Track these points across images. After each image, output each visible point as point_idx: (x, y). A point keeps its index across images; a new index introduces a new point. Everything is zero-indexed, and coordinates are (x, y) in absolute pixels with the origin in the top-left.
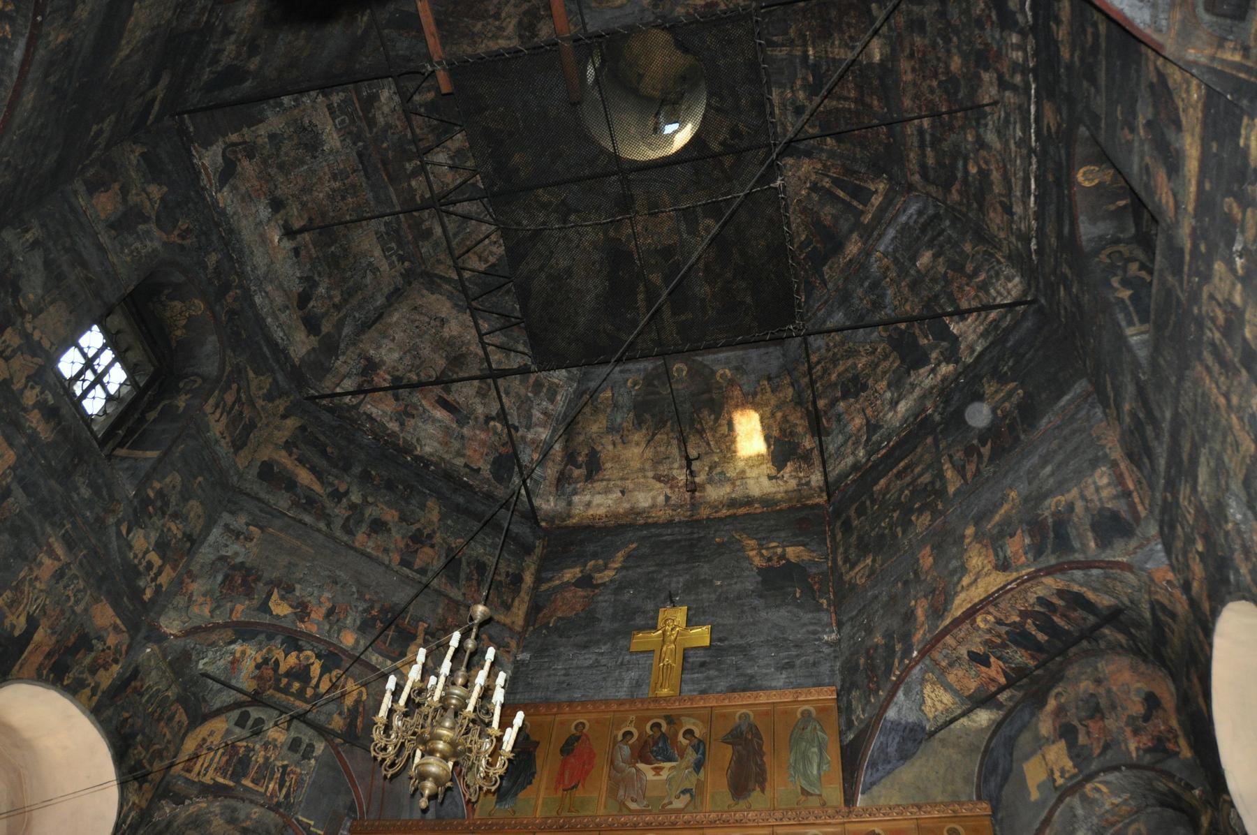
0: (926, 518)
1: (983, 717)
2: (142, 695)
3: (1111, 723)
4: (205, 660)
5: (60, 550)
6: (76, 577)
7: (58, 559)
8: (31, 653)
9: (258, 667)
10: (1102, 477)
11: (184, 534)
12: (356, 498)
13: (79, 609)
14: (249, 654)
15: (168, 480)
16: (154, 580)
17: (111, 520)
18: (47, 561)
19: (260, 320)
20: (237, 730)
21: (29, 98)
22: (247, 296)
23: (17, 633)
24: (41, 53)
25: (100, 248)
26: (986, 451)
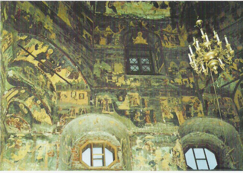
2: (213, 103)
4: (218, 84)
5: (164, 98)
6: (172, 99)
7: (165, 99)
8: (179, 118)
9: (231, 74)
11: (187, 69)
13: (180, 103)
15: (171, 65)
16: (190, 83)
17: (168, 83)
19: (153, 20)
21: (64, 48)
22: (146, 20)
23: (173, 117)
24: (55, 42)
25: (111, 49)
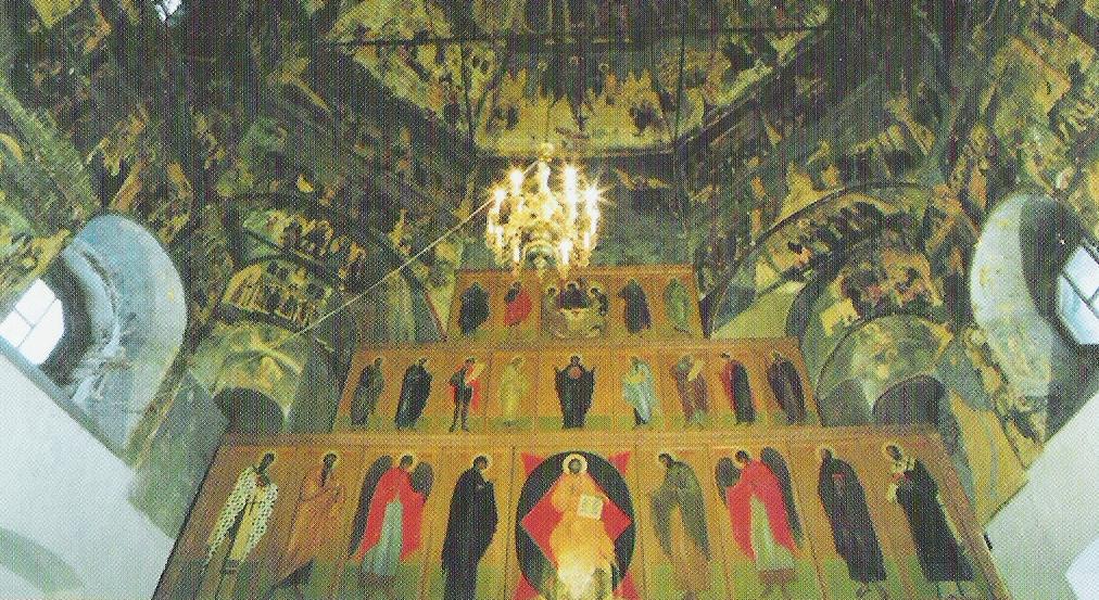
0: (755, 161)
1: (793, 287)
3: (884, 287)
5: (143, 113)
10: (894, 132)
12: (352, 119)
13: (159, 165)
14: (281, 220)
18: (136, 122)
20: (269, 275)
26: (799, 119)
